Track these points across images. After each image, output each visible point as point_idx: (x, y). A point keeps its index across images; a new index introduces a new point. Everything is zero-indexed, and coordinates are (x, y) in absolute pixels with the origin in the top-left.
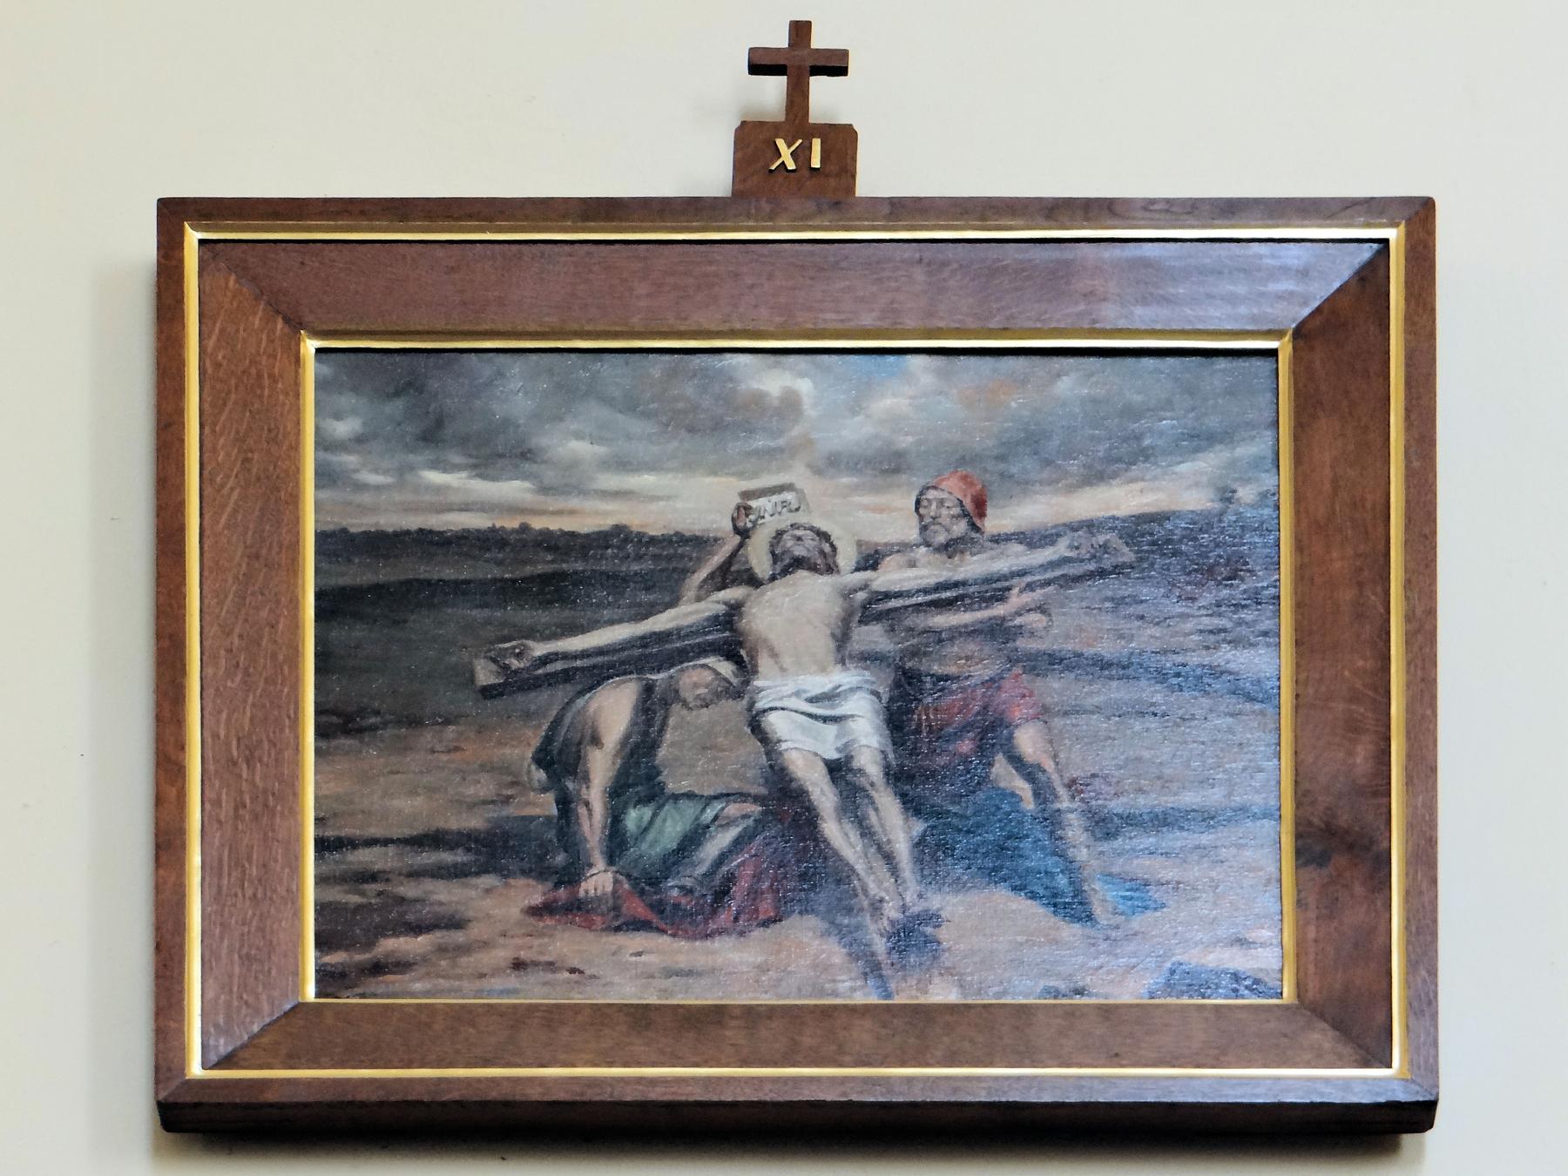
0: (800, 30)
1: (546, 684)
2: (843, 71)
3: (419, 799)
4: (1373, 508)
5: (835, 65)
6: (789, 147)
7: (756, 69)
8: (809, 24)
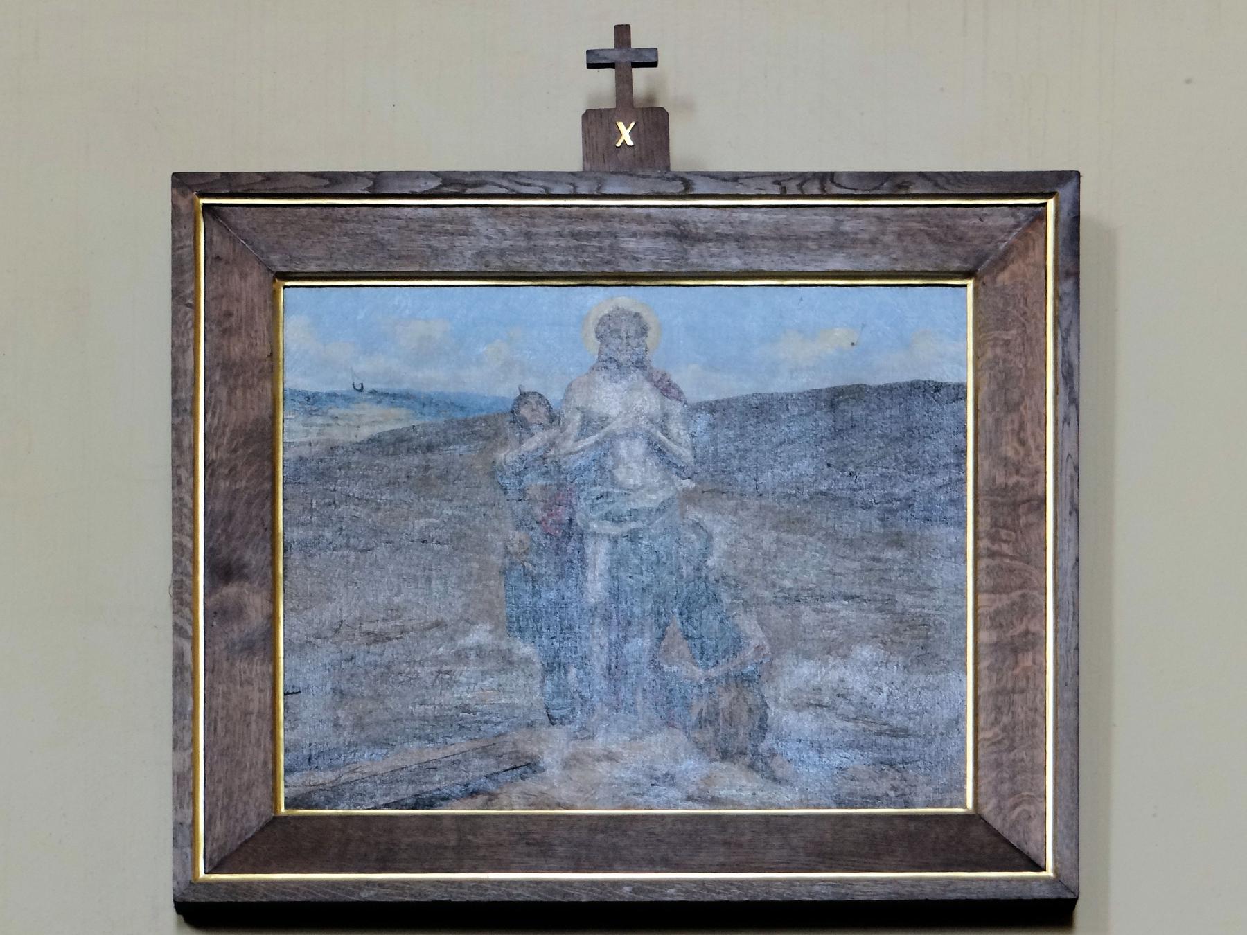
0: (623, 32)
1: (747, 760)
2: (654, 64)
3: (903, 551)
4: (436, 252)
5: (649, 61)
6: (627, 128)
7: (591, 66)
8: (628, 27)
